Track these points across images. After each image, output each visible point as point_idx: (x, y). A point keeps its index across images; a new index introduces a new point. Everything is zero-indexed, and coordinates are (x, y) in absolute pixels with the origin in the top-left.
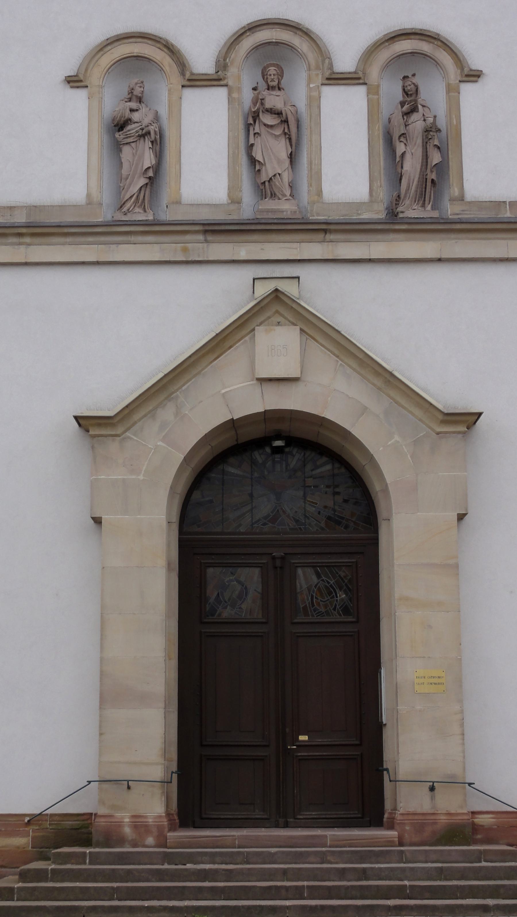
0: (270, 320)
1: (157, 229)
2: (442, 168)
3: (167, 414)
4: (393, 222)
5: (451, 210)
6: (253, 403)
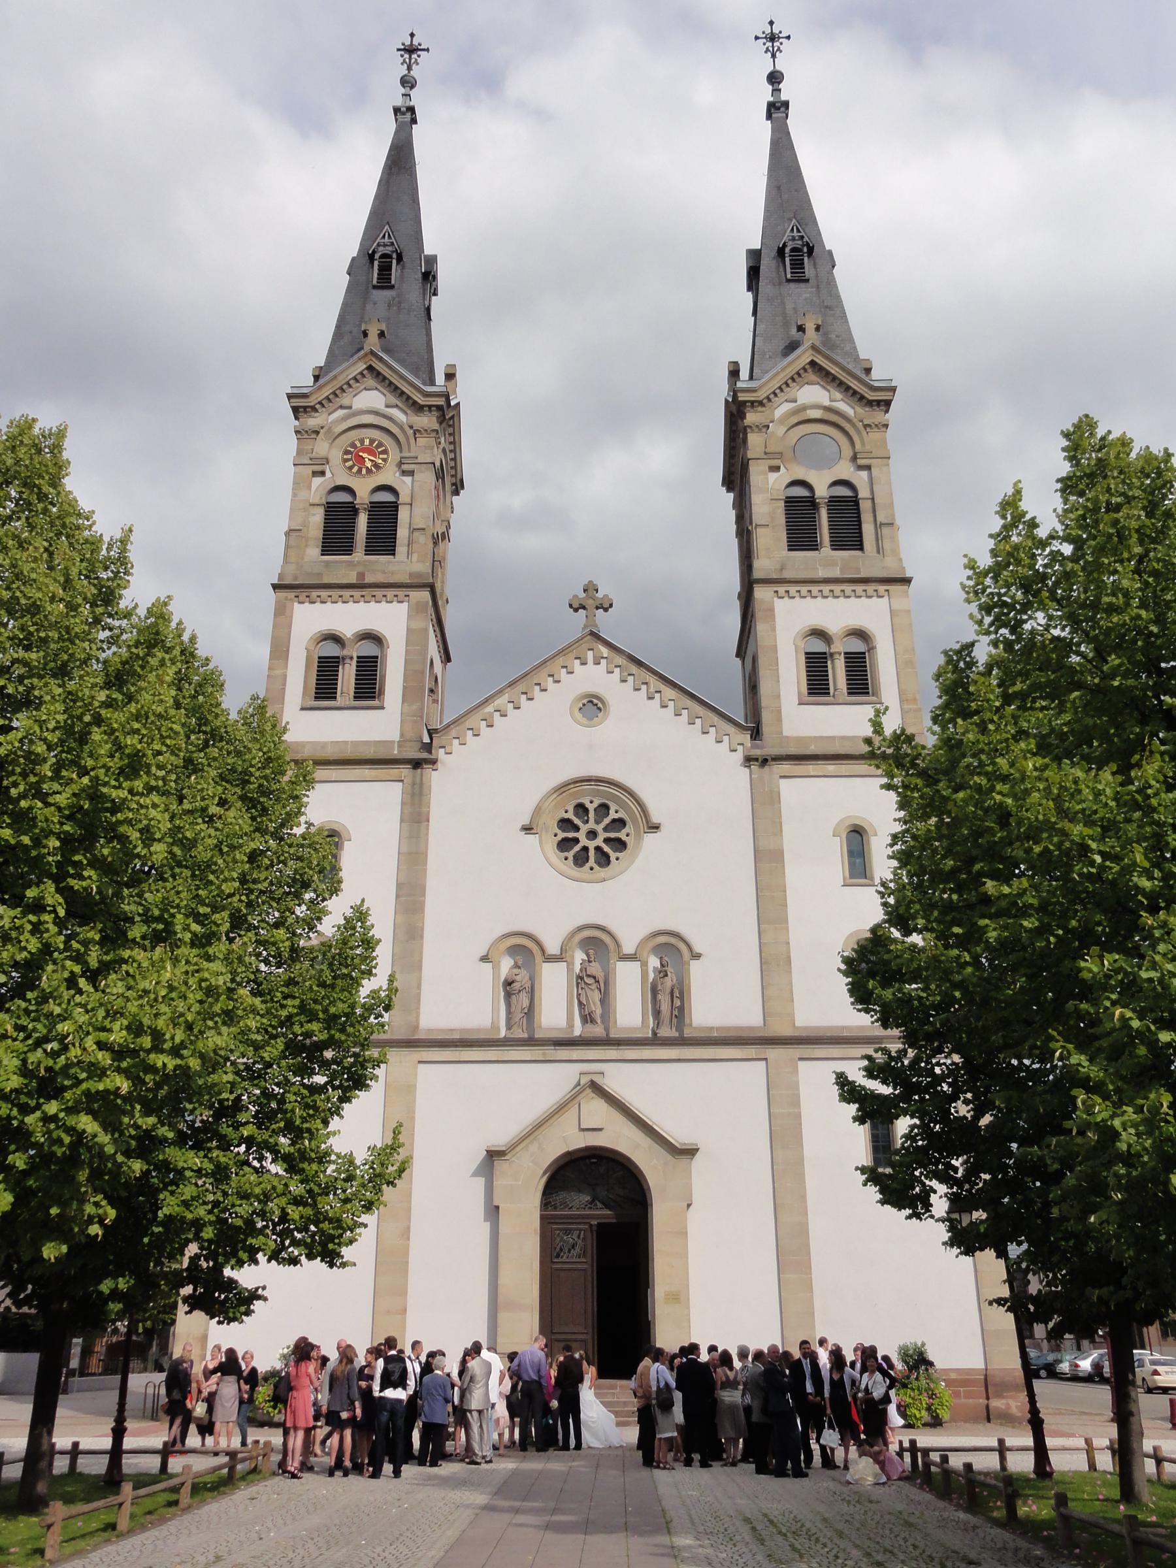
0: (775, 1520)
1: (531, 1042)
2: (681, 1009)
3: (534, 1147)
4: (655, 1041)
5: (687, 1033)
6: (579, 1142)
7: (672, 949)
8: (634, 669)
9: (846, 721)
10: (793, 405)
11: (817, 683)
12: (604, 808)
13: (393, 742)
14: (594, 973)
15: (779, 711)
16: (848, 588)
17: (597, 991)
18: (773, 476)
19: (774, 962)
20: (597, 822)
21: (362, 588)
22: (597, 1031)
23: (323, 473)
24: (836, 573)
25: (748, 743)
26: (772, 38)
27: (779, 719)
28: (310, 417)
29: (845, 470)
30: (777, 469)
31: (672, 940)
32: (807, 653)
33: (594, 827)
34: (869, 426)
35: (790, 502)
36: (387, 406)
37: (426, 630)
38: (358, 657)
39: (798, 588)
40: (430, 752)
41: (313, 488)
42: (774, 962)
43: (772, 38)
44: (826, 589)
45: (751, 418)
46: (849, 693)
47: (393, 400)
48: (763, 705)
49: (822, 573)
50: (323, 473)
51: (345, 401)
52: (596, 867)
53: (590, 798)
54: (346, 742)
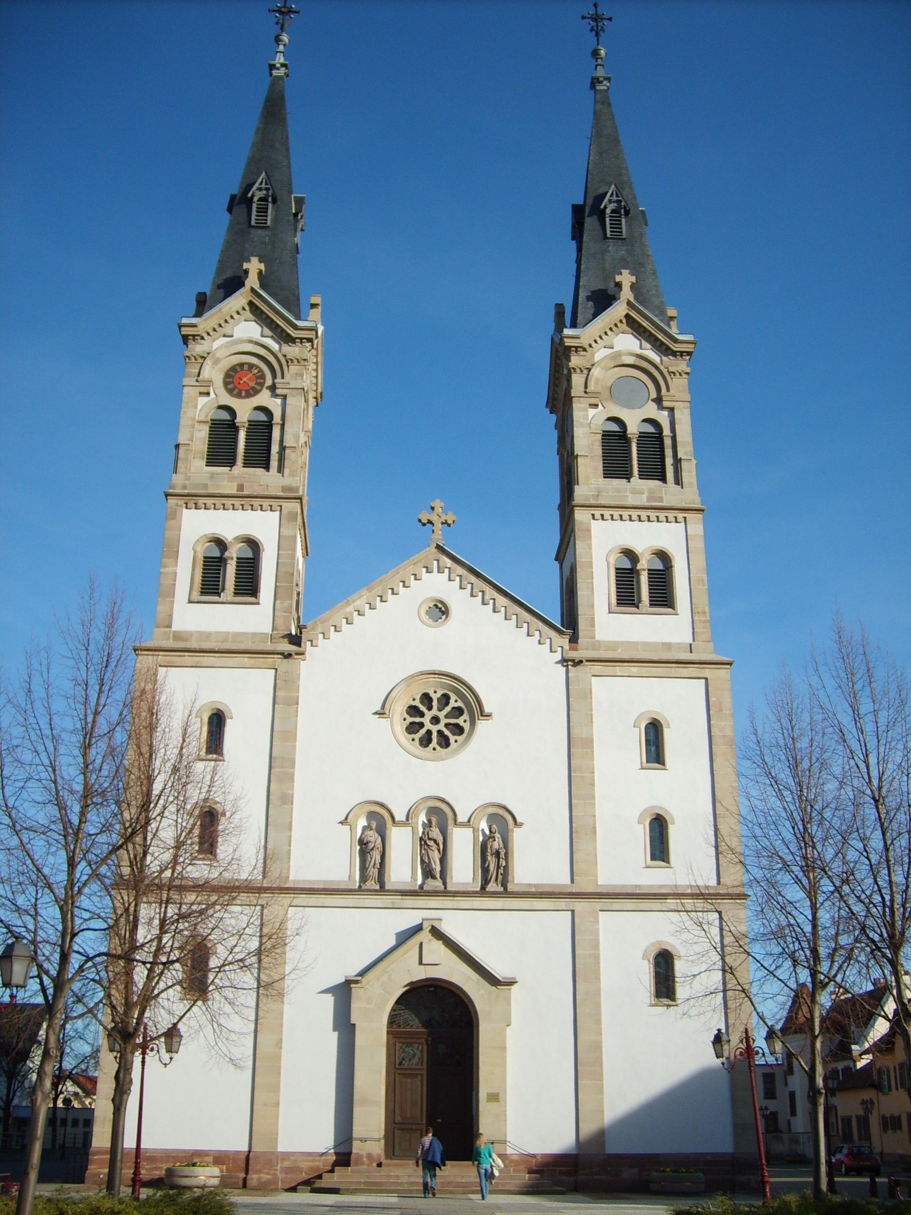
2: (506, 868)
4: (483, 891)
6: (421, 974)
7: (502, 820)
8: (473, 579)
9: (645, 628)
10: (611, 351)
11: (626, 595)
12: (445, 699)
13: (266, 634)
14: (435, 837)
15: (593, 619)
16: (653, 514)
17: (436, 851)
18: (592, 412)
19: (579, 832)
20: (440, 710)
21: (245, 499)
22: (437, 884)
23: (208, 394)
24: (643, 500)
25: (567, 646)
26: (596, 18)
27: (593, 625)
28: (198, 343)
29: (651, 410)
30: (596, 406)
31: (501, 812)
32: (617, 569)
33: (442, 714)
34: (674, 373)
35: (607, 436)
36: (262, 336)
37: (296, 536)
38: (238, 558)
39: (611, 513)
40: (299, 645)
41: (199, 407)
42: (579, 832)
43: (596, 18)
44: (634, 514)
45: (575, 361)
46: (651, 605)
47: (267, 331)
48: (580, 612)
49: (631, 500)
50: (208, 394)
51: (227, 329)
52: (438, 747)
53: (456, 698)
54: (228, 633)
